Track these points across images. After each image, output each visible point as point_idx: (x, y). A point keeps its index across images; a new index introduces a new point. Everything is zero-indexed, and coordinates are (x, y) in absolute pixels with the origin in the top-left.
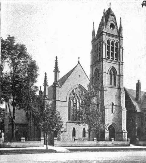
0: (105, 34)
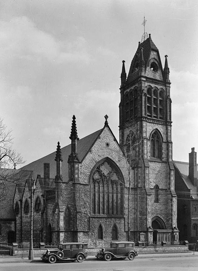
0: (145, 79)
